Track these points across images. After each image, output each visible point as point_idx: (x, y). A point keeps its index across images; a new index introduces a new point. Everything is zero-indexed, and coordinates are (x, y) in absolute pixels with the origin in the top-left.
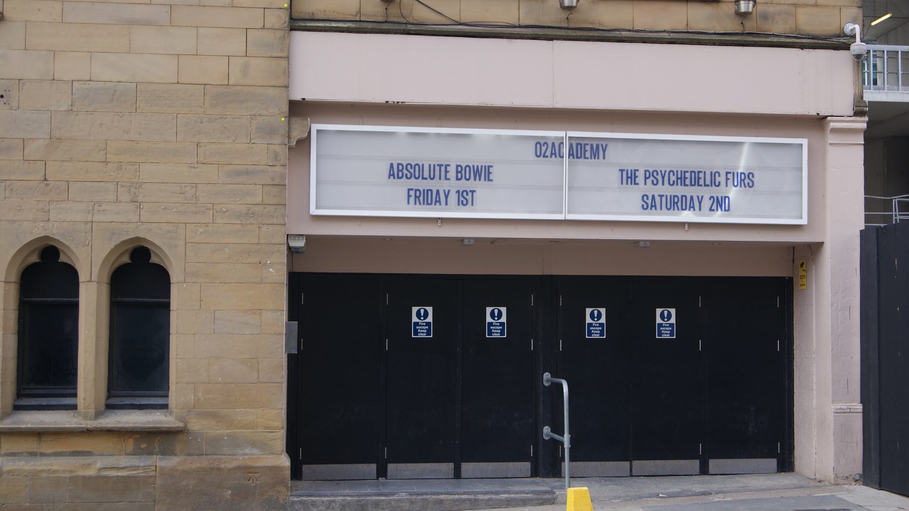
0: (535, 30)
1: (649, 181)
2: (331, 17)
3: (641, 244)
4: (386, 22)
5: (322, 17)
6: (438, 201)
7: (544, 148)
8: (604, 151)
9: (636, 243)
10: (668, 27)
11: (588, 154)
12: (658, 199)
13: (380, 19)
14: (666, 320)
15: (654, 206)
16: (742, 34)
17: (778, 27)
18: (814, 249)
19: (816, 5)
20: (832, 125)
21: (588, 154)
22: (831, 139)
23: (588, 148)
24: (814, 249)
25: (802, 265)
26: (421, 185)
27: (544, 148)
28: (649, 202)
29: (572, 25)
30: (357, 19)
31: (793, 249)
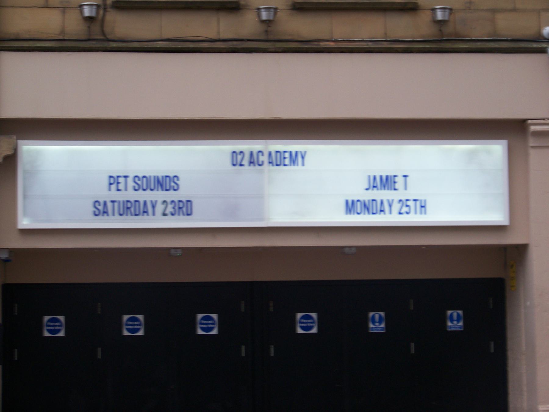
0: (235, 43)
1: (114, 187)
2: (36, 37)
3: (347, 250)
4: (89, 40)
5: (27, 36)
6: (145, 212)
7: (239, 157)
8: (303, 158)
9: (340, 249)
10: (366, 37)
11: (287, 161)
12: (109, 205)
13: (83, 37)
14: (377, 323)
15: (105, 212)
16: (440, 41)
17: (479, 31)
18: (519, 252)
19: (514, 10)
20: (533, 128)
21: (287, 161)
22: (532, 142)
23: (287, 155)
24: (519, 252)
25: (512, 266)
26: (170, 196)
27: (239, 157)
28: (101, 208)
29: (271, 37)
30: (61, 38)
31: (504, 249)
